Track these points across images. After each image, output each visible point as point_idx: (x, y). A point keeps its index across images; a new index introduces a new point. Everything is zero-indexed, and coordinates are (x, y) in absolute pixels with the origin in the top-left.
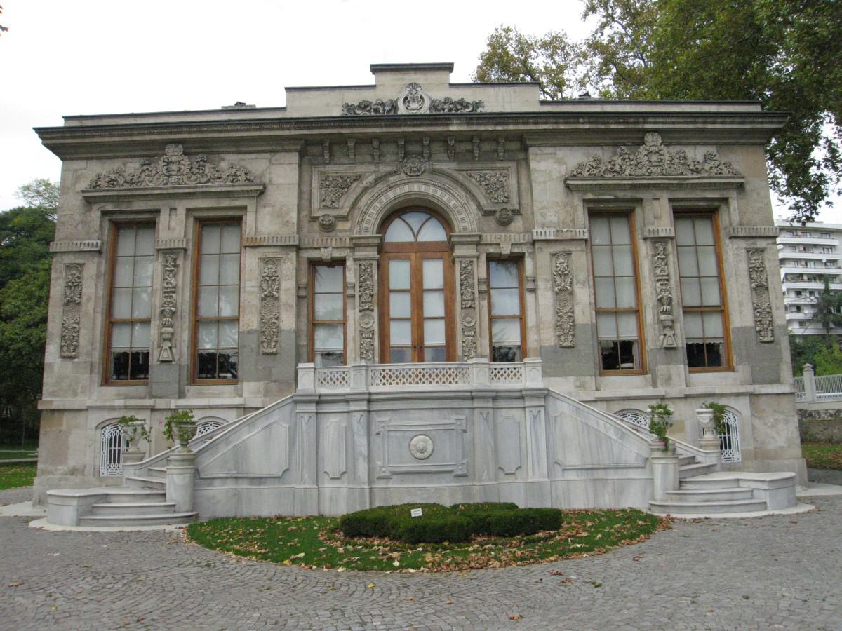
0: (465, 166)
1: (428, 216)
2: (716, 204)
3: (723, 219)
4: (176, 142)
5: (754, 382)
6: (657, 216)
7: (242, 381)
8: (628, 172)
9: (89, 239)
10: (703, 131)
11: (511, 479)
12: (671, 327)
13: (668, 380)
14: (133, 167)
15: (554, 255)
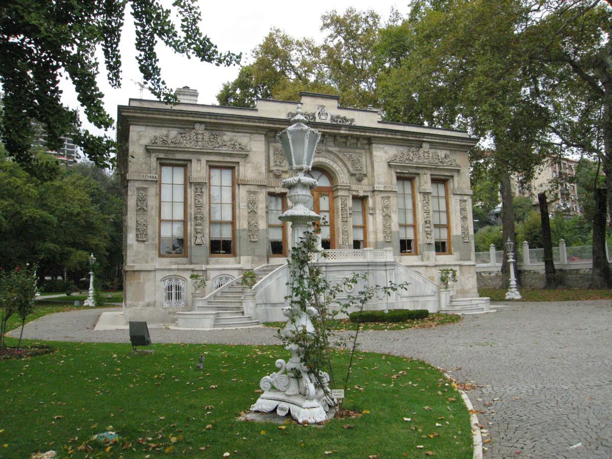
0: (343, 150)
1: (321, 173)
2: (448, 178)
3: (450, 185)
4: (201, 123)
5: (461, 260)
6: (425, 182)
7: (240, 256)
8: (415, 161)
9: (150, 173)
10: (445, 144)
11: (381, 302)
12: (430, 234)
13: (428, 258)
14: (173, 133)
15: (382, 198)
